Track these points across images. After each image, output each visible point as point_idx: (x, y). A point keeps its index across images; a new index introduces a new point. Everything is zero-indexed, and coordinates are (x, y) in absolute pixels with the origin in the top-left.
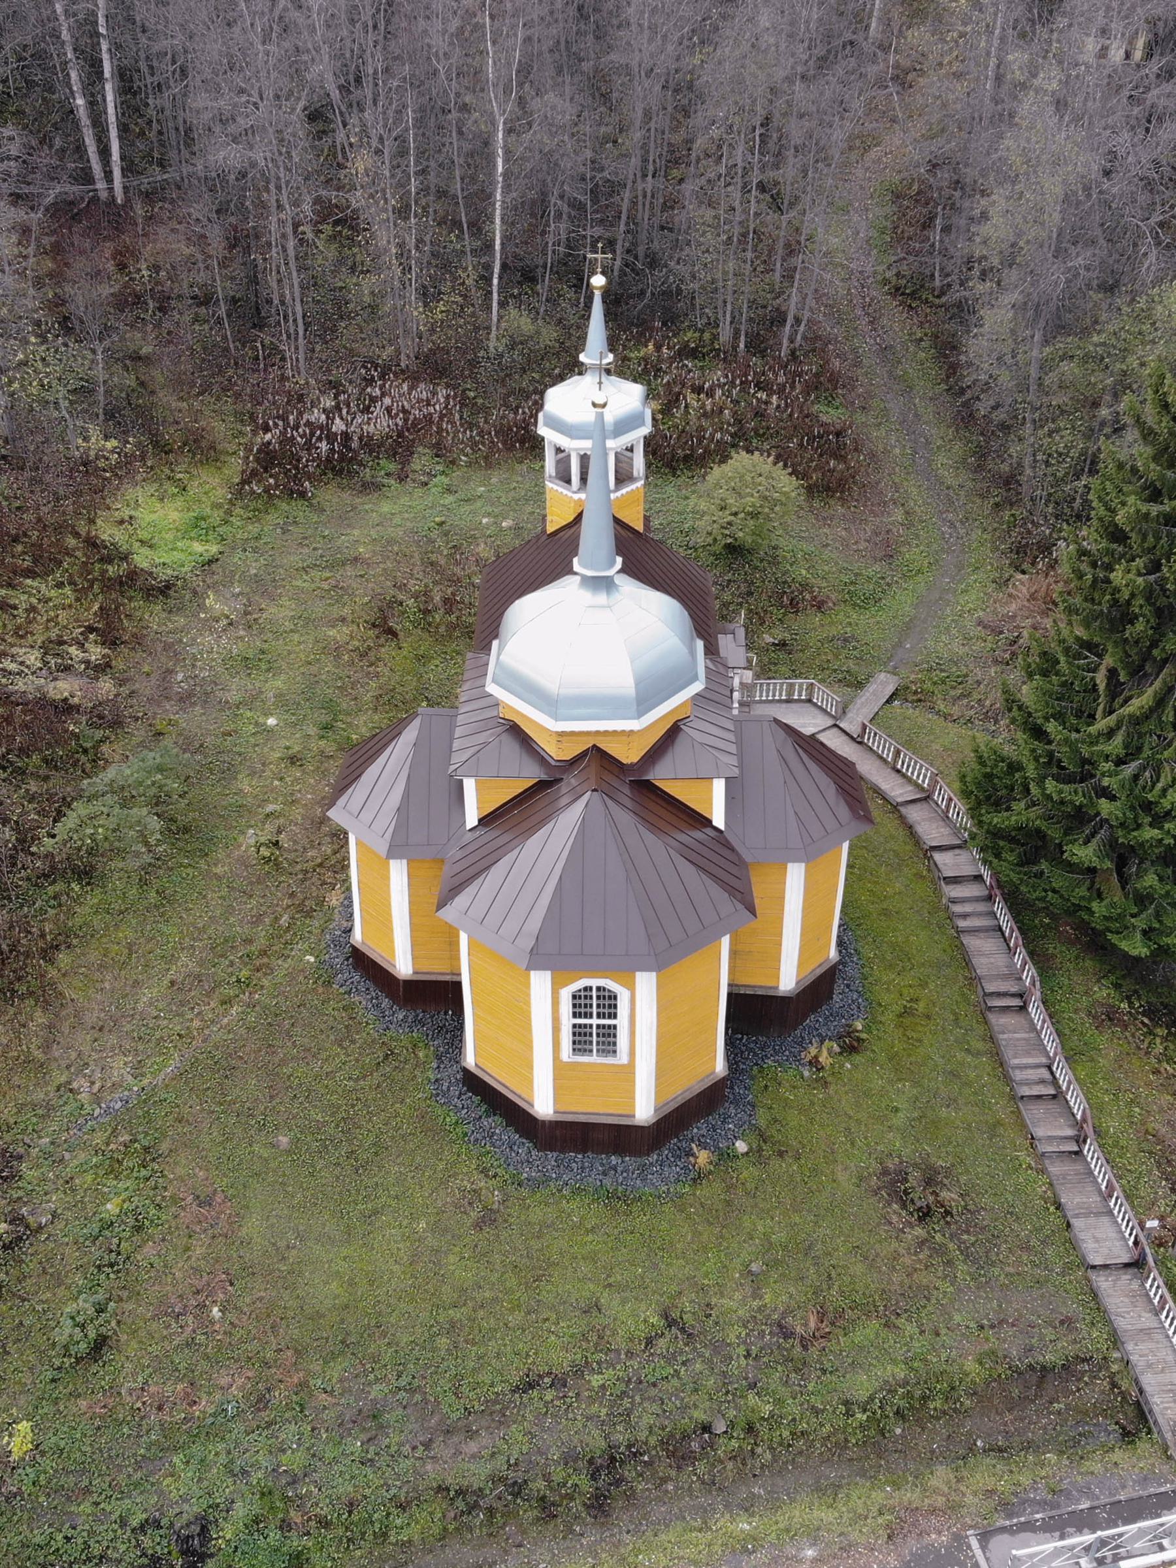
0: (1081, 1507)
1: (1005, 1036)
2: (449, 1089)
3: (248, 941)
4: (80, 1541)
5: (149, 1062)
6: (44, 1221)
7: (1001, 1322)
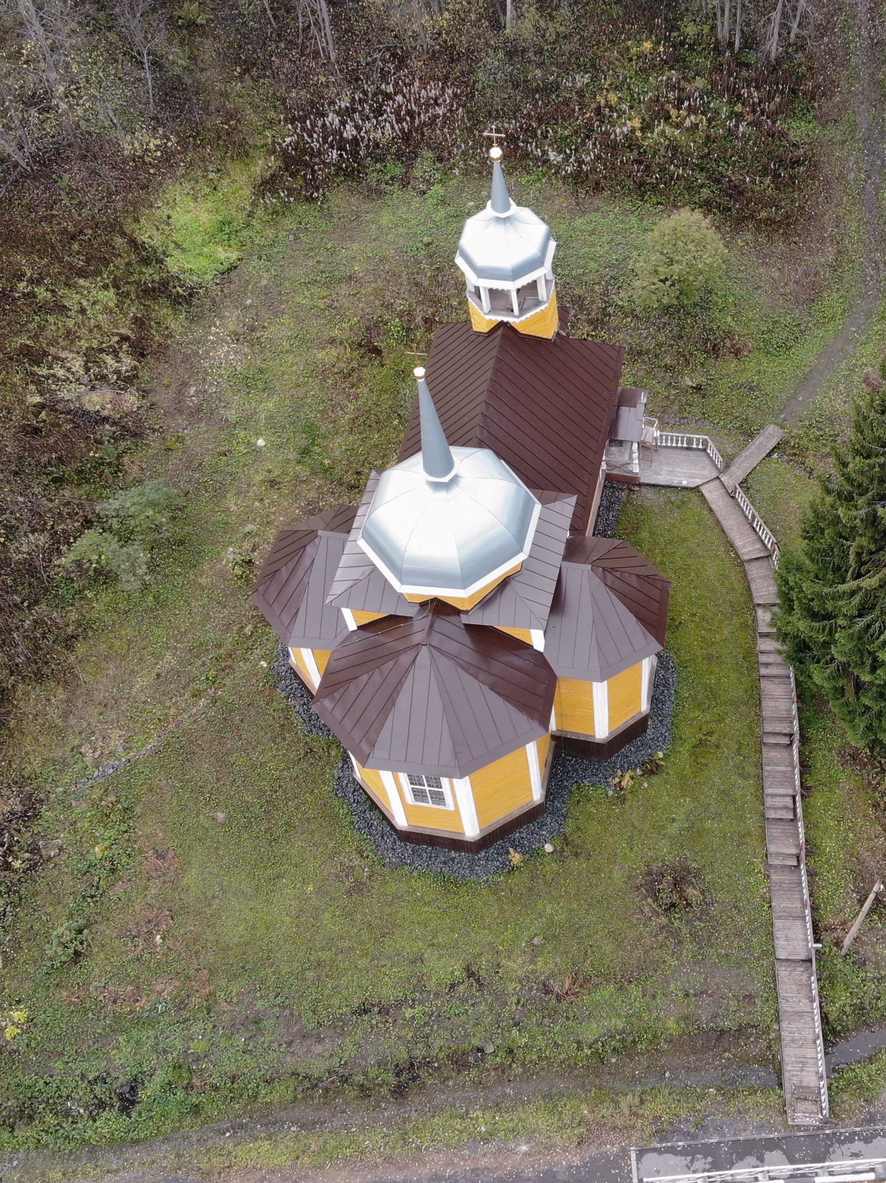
0: (711, 1141)
1: (769, 768)
2: (347, 786)
3: (219, 646)
4: (54, 1085)
5: (136, 738)
6: (52, 855)
7: (702, 993)
